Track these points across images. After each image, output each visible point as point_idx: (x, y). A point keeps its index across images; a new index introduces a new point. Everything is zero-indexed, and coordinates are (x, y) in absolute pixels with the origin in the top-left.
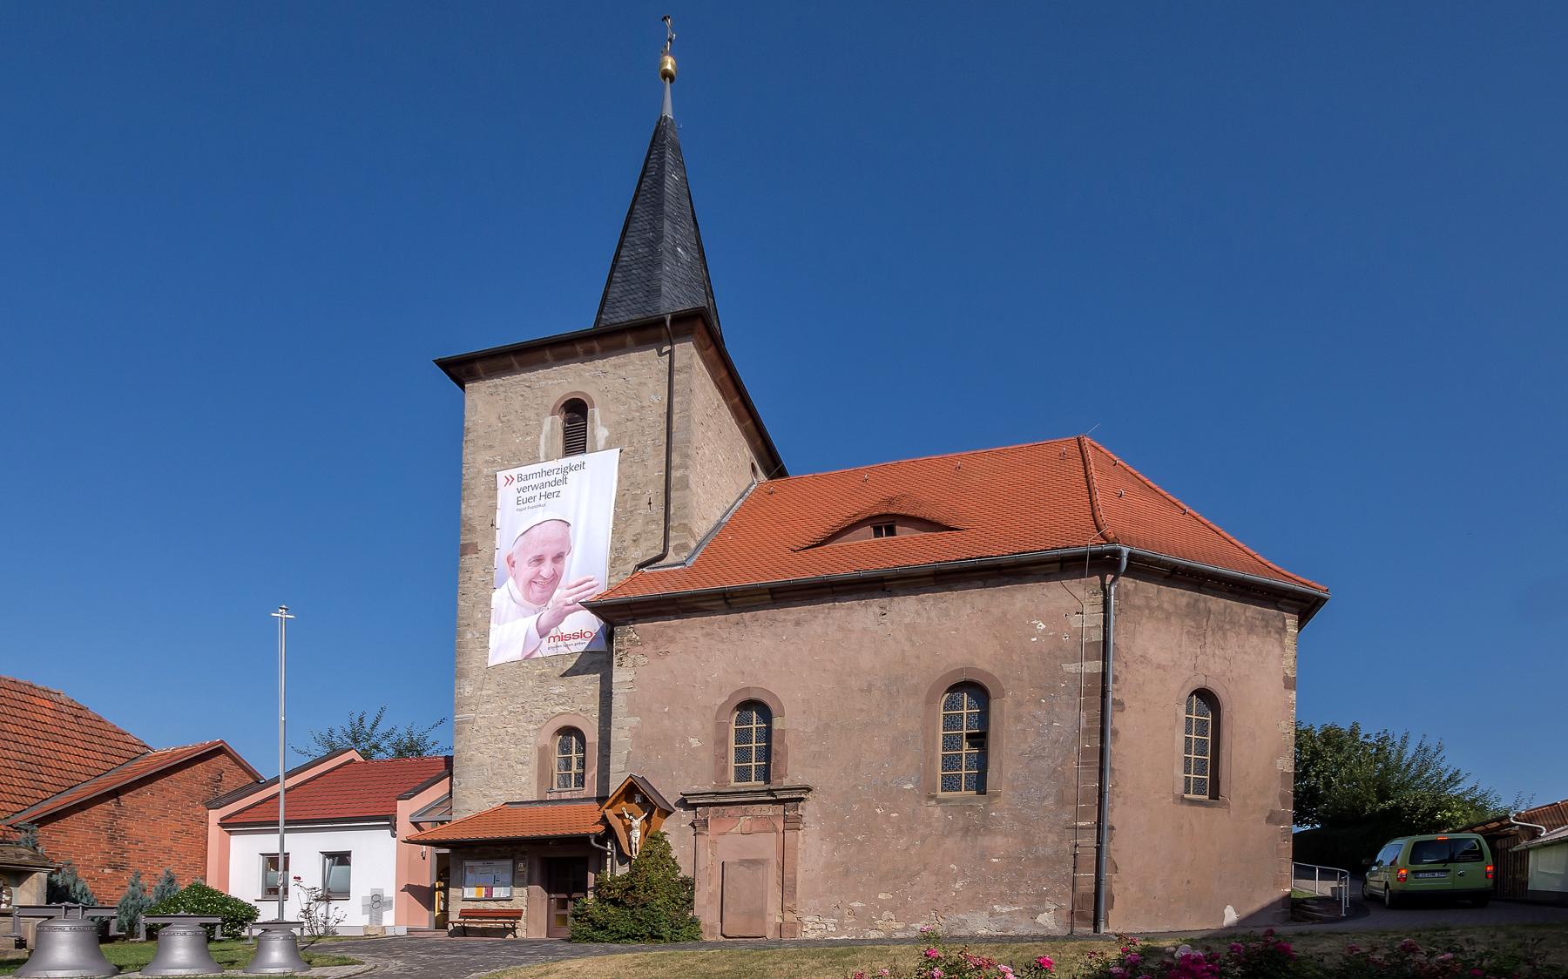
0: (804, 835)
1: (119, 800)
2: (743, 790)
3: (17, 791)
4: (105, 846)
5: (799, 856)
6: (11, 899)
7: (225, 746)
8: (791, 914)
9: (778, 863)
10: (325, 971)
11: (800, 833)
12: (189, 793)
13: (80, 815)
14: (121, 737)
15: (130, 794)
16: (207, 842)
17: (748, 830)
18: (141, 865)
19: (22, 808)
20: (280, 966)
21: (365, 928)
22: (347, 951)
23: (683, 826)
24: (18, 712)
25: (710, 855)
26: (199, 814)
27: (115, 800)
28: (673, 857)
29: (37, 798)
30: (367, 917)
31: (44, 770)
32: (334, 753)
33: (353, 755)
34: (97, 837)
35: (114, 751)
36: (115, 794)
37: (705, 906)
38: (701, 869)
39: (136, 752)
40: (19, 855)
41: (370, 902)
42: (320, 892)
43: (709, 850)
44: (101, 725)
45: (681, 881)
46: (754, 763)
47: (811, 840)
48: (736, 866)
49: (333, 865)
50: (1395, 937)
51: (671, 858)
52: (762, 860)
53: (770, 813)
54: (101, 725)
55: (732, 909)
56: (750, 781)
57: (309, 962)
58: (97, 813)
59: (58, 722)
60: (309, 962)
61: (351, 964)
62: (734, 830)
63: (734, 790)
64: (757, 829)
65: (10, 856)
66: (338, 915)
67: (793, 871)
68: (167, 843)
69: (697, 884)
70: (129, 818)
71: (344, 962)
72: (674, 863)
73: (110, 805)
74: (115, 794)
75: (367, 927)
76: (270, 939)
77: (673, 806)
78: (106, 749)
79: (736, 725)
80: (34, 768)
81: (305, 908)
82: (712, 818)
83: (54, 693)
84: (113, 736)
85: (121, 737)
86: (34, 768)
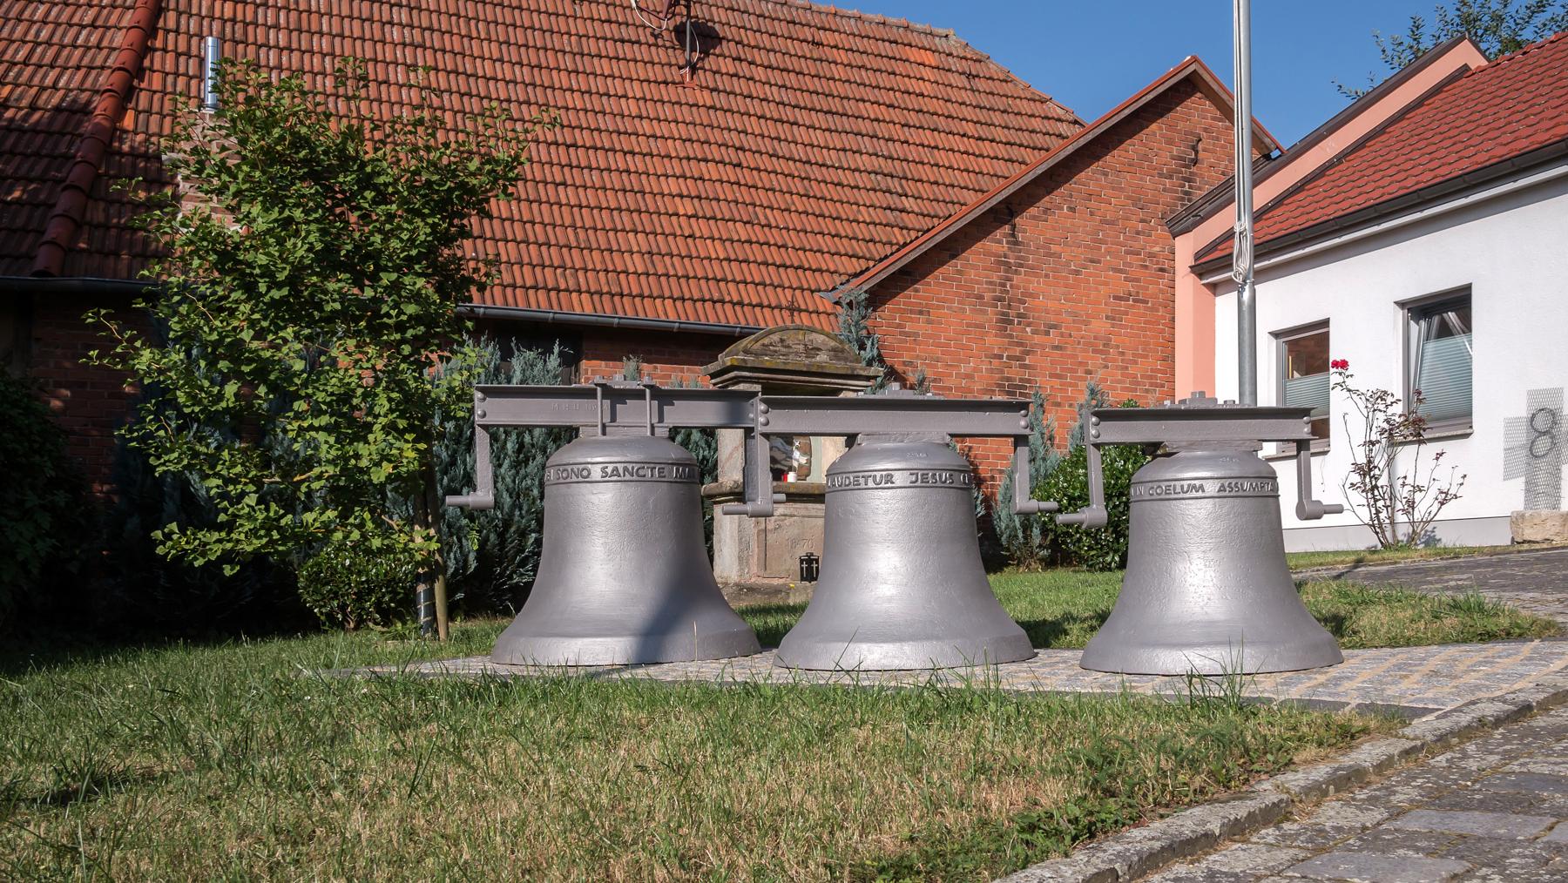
1: (1014, 227)
3: (862, 231)
4: (993, 341)
6: (809, 462)
7: (1201, 71)
10: (1404, 670)
12: (1138, 202)
13: (948, 269)
14: (1037, 108)
15: (1033, 211)
16: (1173, 320)
18: (1056, 383)
19: (863, 264)
20: (1210, 636)
21: (1516, 520)
22: (1483, 584)
24: (883, 80)
26: (1157, 249)
27: (1007, 229)
29: (891, 244)
30: (1519, 483)
31: (910, 187)
32: (1421, 61)
33: (1465, 55)
34: (980, 319)
35: (1025, 138)
36: (1005, 213)
39: (1059, 136)
40: (812, 351)
41: (1522, 438)
42: (1398, 409)
44: (1007, 89)
49: (1428, 338)
50: (426, 668)
54: (1007, 89)
57: (1337, 625)
58: (978, 261)
59: (942, 91)
60: (1337, 625)
61: (1508, 635)
65: (797, 353)
66: (1445, 478)
68: (1100, 326)
70: (1033, 270)
71: (1481, 623)
73: (996, 243)
74: (1005, 213)
75: (1523, 516)
76: (1168, 495)
78: (1013, 136)
80: (894, 184)
81: (1362, 460)
83: (941, 37)
84: (1026, 107)
85: (1037, 108)
86: (894, 184)
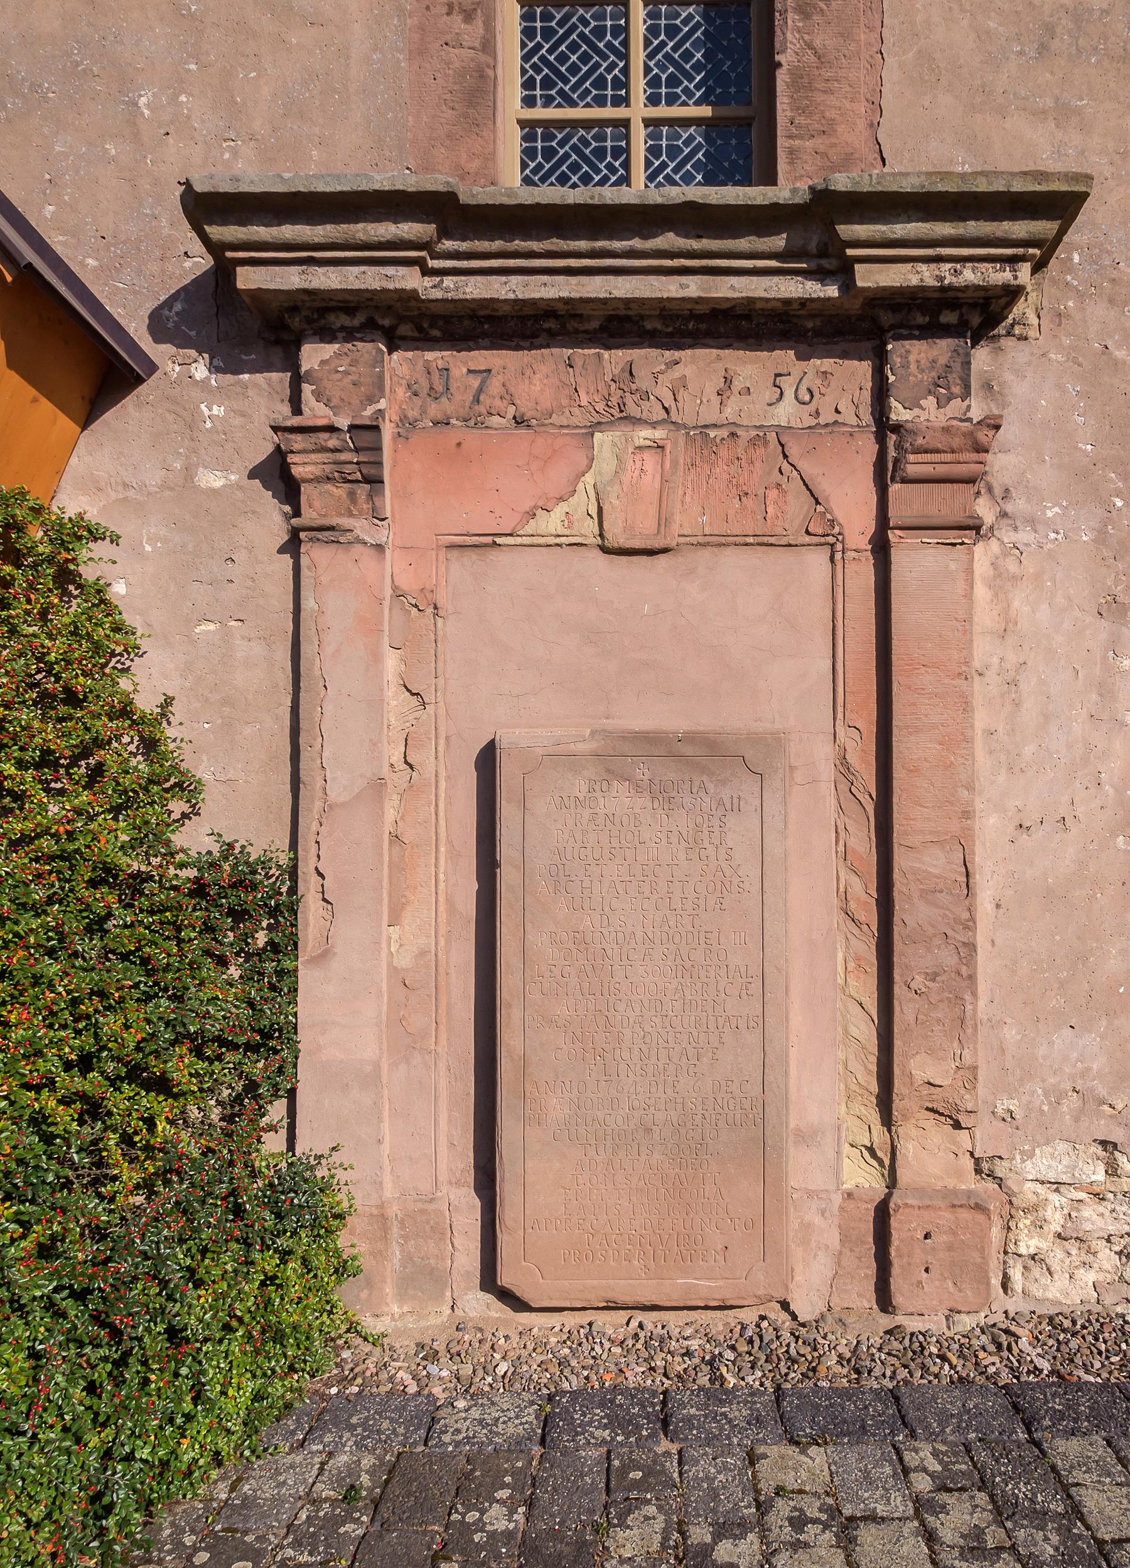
0: (1000, 581)
2: (668, 240)
5: (981, 720)
8: (937, 1133)
9: (843, 764)
11: (983, 553)
17: (644, 534)
23: (212, 480)
25: (396, 700)
28: (146, 703)
37: (372, 1079)
38: (335, 794)
43: (392, 662)
45: (199, 889)
46: (638, 110)
47: (1044, 613)
48: (580, 788)
51: (125, 711)
52: (756, 739)
53: (786, 412)
55: (557, 1107)
56: (625, 180)
62: (551, 523)
63: (319, 535)
64: (707, 523)
67: (955, 826)
69: (311, 912)
72: (150, 745)
77: (137, 329)
79: (529, 102)
82: (407, 425)
